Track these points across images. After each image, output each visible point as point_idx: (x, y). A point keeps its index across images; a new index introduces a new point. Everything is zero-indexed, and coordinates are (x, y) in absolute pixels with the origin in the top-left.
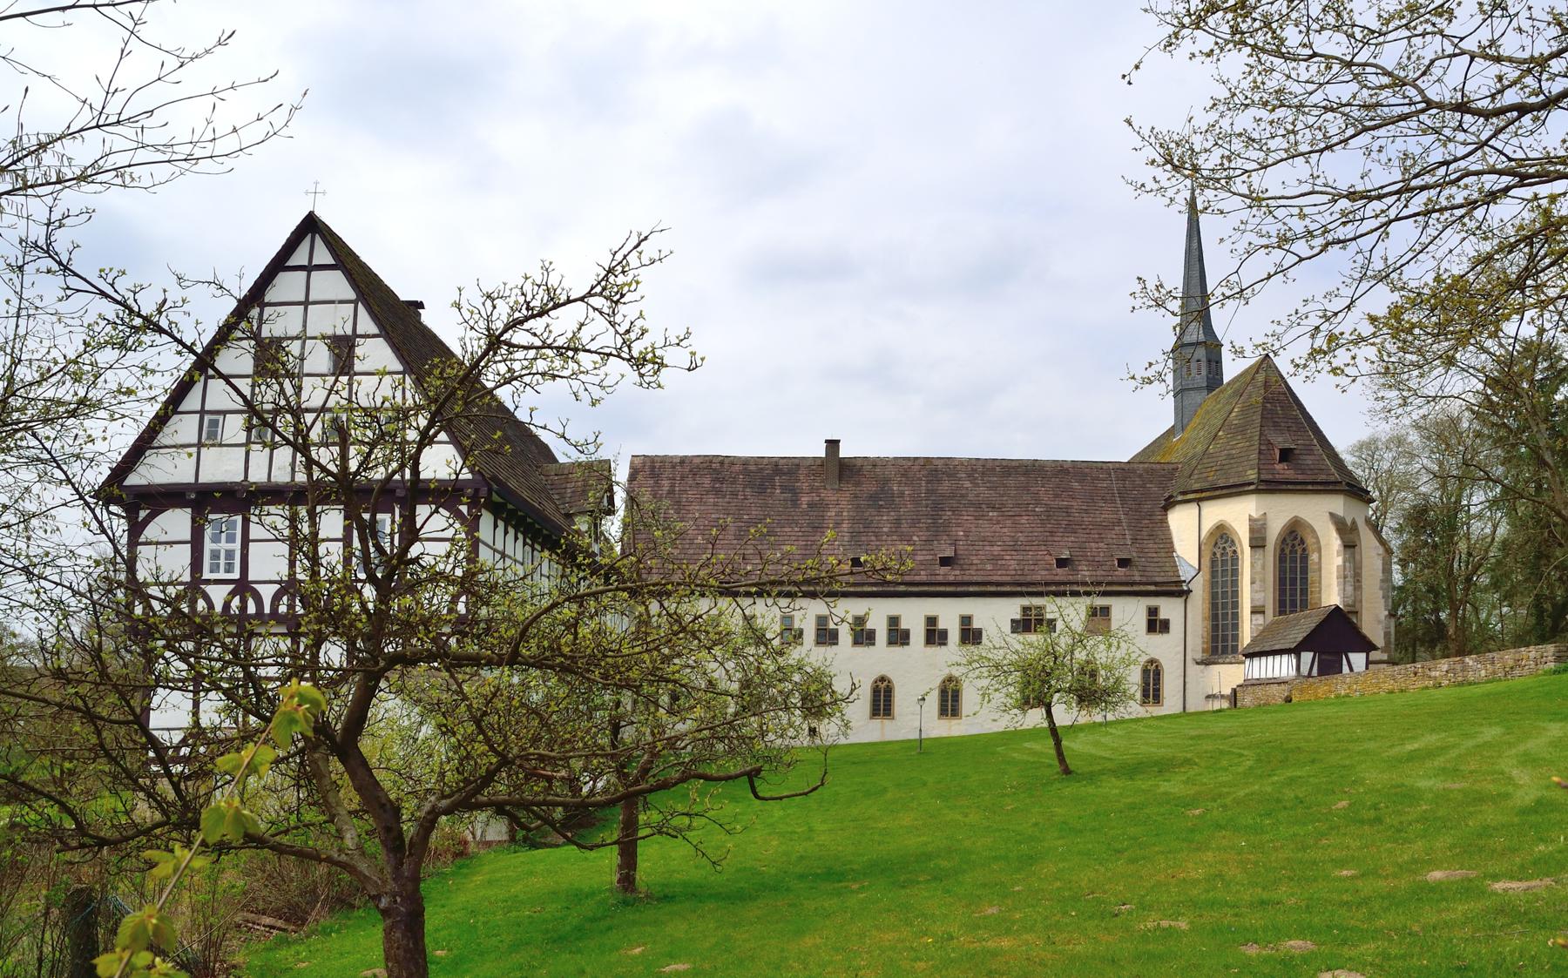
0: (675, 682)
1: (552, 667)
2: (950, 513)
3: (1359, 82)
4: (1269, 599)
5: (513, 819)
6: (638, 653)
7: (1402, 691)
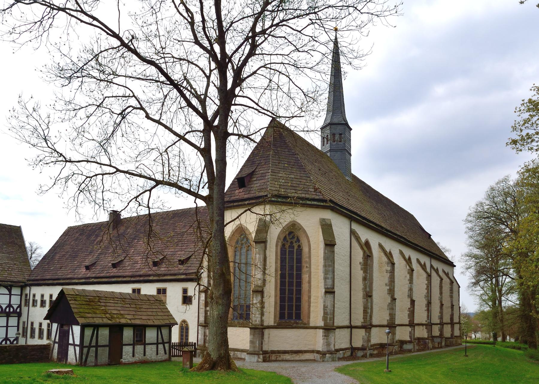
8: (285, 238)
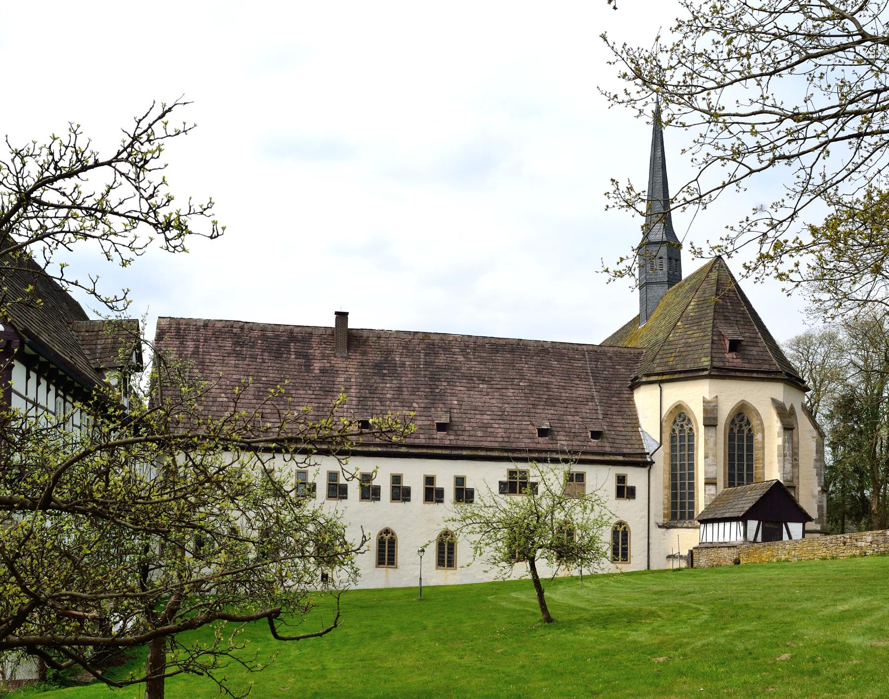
0: (202, 528)
1: (84, 512)
2: (445, 384)
3: (804, 13)
4: (720, 473)
5: (44, 658)
6: (166, 501)
7: (833, 558)
8: (733, 421)
